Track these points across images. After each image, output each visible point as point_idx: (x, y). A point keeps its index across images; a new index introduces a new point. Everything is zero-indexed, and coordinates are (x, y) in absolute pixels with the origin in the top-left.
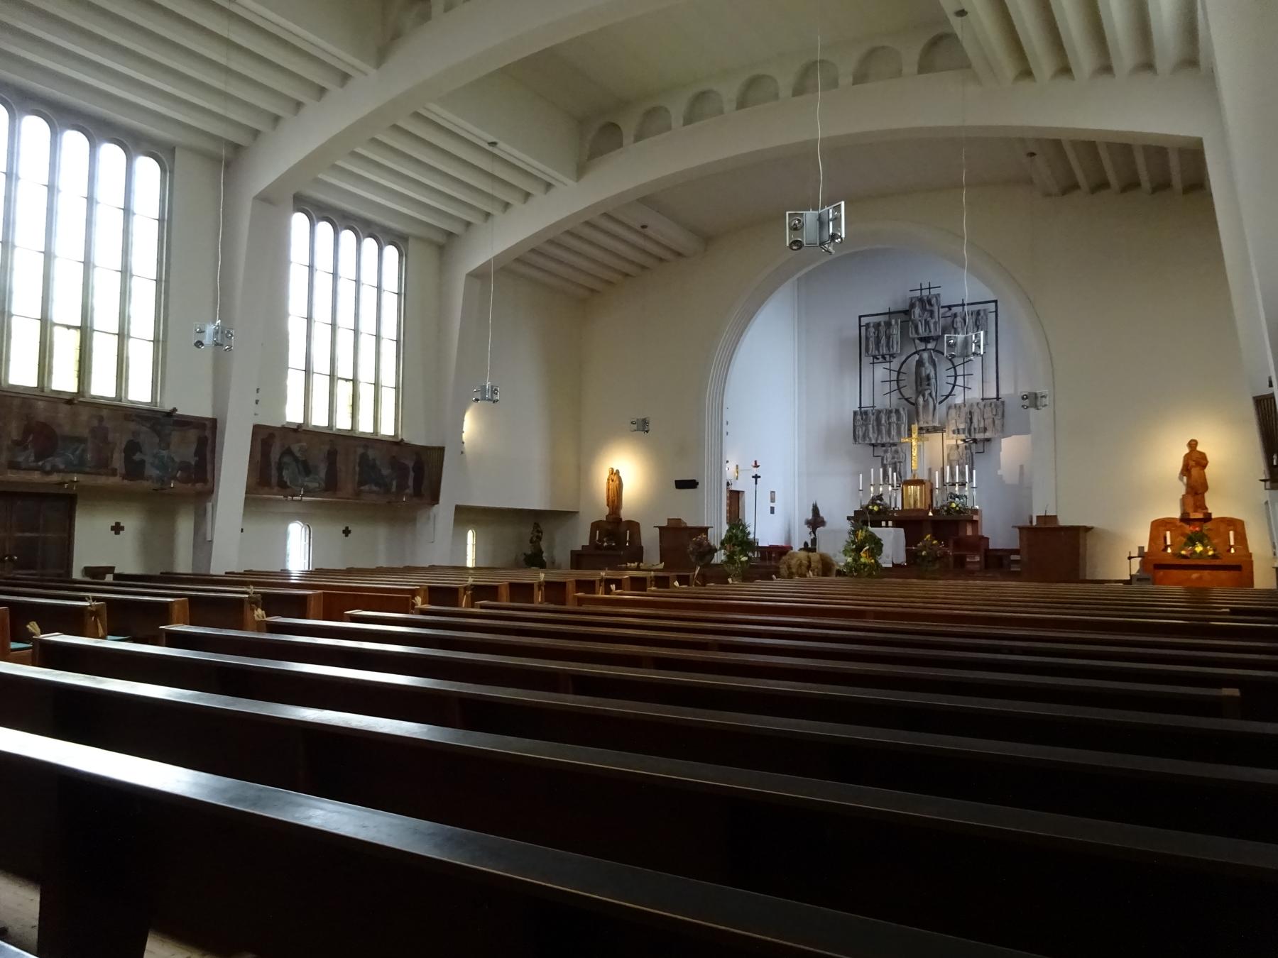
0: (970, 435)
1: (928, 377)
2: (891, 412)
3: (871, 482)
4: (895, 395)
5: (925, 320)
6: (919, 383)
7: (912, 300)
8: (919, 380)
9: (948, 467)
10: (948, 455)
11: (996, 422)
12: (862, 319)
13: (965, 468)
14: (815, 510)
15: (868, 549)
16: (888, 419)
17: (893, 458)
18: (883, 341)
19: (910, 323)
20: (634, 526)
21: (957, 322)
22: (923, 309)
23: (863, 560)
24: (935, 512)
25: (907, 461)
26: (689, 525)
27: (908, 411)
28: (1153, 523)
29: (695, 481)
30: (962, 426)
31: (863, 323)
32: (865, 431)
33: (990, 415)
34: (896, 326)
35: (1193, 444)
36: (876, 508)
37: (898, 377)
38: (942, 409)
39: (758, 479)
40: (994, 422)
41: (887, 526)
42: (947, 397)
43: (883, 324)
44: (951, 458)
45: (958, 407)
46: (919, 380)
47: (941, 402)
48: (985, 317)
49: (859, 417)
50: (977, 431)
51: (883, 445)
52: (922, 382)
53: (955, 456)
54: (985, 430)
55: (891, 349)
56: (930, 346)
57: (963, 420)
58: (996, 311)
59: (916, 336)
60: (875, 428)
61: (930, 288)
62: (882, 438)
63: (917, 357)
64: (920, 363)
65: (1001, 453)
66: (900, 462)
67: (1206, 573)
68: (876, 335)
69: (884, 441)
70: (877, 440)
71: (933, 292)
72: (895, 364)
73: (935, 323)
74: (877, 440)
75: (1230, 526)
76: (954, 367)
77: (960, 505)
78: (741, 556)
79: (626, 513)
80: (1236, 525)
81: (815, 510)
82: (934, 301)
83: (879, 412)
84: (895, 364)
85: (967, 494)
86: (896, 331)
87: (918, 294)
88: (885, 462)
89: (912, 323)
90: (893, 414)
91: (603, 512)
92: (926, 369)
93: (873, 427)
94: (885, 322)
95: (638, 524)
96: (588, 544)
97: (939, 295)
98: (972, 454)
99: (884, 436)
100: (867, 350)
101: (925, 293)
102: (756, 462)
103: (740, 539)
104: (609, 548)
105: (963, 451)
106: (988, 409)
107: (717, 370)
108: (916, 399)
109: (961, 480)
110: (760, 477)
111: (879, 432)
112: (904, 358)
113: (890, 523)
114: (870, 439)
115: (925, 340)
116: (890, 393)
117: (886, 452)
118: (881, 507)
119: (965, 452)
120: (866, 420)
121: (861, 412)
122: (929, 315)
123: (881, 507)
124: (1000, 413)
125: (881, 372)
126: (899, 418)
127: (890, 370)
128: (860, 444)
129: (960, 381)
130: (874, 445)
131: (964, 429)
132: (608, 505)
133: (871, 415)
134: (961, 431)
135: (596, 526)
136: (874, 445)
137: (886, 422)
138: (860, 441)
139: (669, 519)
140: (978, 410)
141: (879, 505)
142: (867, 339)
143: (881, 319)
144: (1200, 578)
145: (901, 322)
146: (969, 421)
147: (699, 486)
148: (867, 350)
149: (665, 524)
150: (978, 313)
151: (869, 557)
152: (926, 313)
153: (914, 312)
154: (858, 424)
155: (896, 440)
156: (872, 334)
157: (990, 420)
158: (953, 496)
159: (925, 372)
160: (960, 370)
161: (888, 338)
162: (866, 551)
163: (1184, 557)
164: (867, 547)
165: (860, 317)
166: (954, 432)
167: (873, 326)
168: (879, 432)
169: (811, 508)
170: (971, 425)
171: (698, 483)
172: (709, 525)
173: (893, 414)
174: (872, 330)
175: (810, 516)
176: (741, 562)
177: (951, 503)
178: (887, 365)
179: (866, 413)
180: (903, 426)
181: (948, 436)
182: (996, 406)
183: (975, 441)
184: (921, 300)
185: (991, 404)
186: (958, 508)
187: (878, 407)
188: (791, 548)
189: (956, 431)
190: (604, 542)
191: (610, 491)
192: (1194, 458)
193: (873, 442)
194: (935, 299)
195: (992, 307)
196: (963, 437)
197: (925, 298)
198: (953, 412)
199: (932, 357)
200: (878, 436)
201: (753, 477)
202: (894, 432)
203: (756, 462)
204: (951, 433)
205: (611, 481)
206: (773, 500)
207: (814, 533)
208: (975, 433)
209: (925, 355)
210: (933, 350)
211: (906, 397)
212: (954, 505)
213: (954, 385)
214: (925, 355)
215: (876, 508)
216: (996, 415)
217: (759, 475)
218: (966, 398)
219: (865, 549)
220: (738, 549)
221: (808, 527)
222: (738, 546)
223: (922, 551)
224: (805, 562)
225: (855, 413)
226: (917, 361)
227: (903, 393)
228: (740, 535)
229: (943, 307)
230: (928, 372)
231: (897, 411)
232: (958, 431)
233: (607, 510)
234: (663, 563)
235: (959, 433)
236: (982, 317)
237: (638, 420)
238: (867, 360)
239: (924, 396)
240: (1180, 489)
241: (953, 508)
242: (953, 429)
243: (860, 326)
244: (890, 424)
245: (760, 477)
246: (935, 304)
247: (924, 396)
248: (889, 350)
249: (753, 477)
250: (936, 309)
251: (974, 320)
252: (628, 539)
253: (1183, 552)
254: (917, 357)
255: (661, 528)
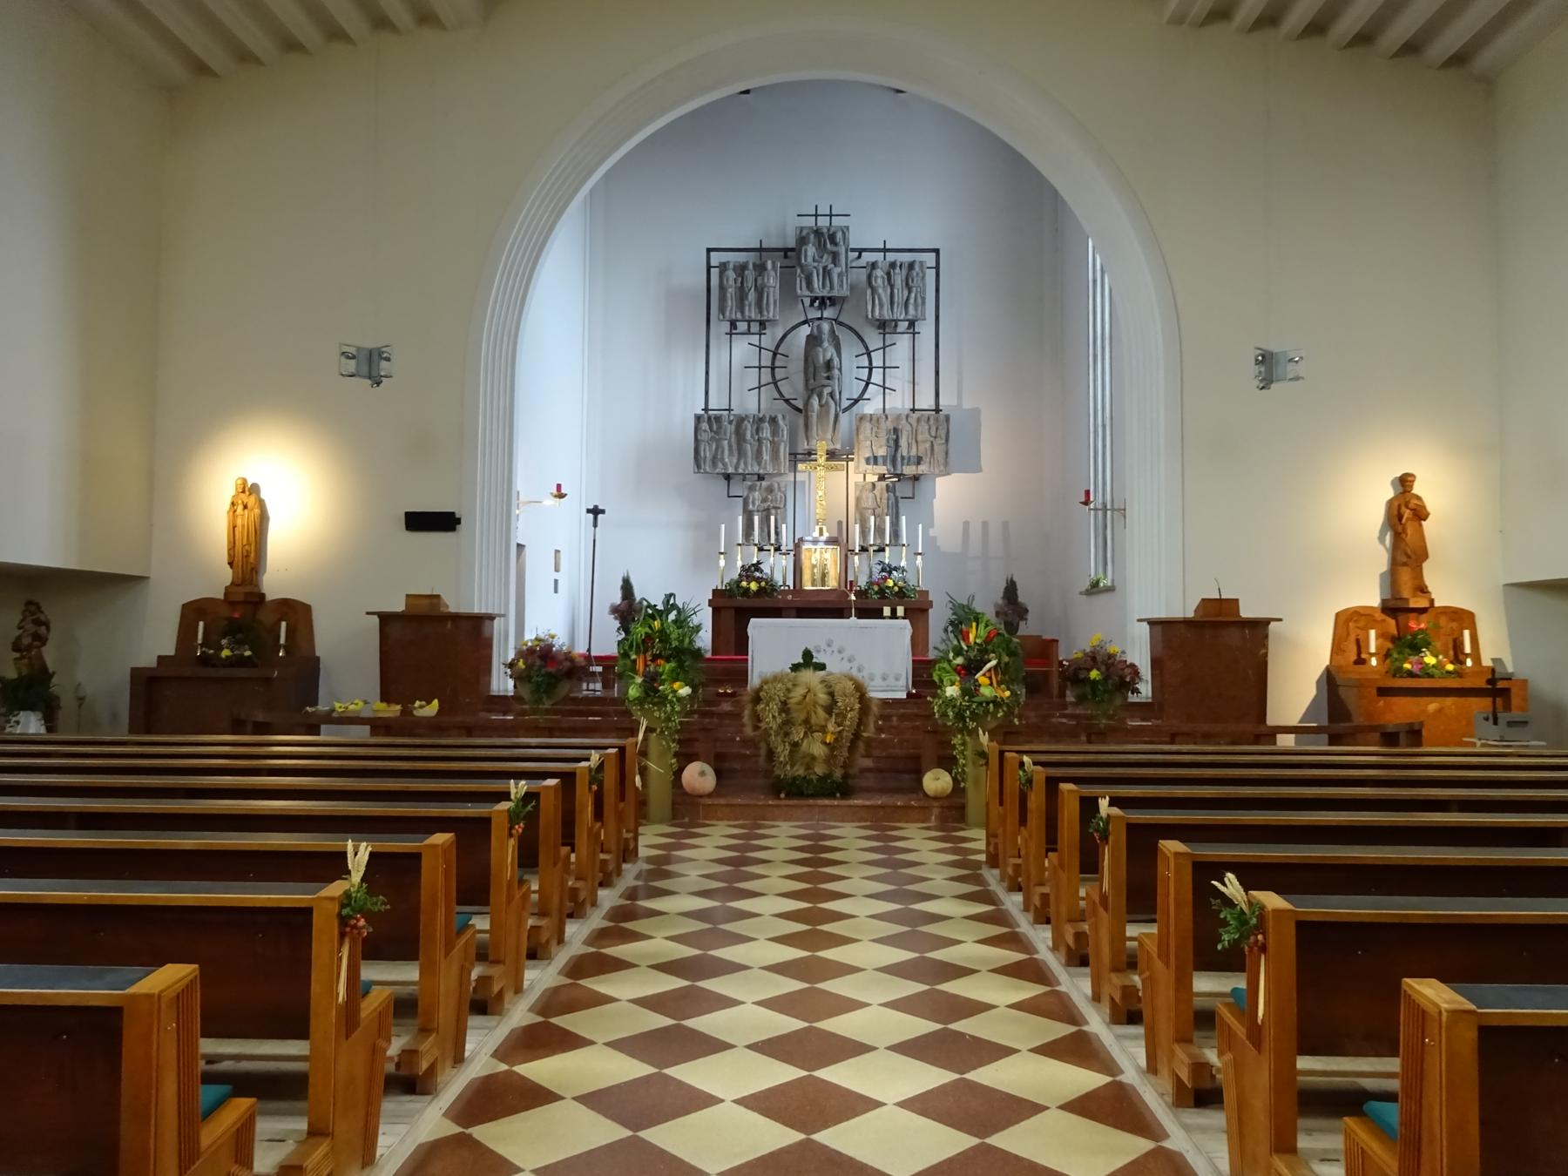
0: (894, 466)
1: (829, 365)
2: (761, 420)
3: (719, 547)
4: (768, 392)
5: (825, 268)
7: (801, 231)
8: (811, 369)
9: (857, 526)
10: (858, 500)
11: (936, 447)
12: (712, 254)
13: (884, 521)
15: (995, 667)
17: (764, 500)
18: (752, 296)
20: (296, 612)
21: (876, 277)
22: (821, 247)
23: (987, 691)
24: (859, 594)
25: (788, 503)
26: (453, 608)
27: (790, 422)
28: (1338, 615)
29: (453, 514)
30: (882, 452)
34: (773, 273)
35: (1405, 482)
36: (754, 586)
37: (773, 362)
39: (600, 516)
41: (894, 615)
42: (856, 401)
43: (751, 266)
44: (864, 505)
45: (874, 418)
46: (811, 369)
48: (921, 275)
49: (705, 426)
50: (906, 461)
51: (744, 477)
52: (818, 373)
53: (869, 502)
54: (919, 460)
55: (765, 313)
56: (829, 313)
57: (883, 440)
58: (937, 268)
59: (808, 293)
60: (735, 447)
62: (746, 464)
64: (813, 341)
65: (935, 501)
66: (776, 508)
67: (1449, 701)
68: (739, 284)
69: (750, 470)
70: (736, 468)
71: (837, 221)
72: (768, 341)
73: (840, 275)
74: (736, 468)
75: (1454, 620)
77: (901, 583)
78: (676, 686)
79: (276, 581)
80: (1463, 618)
82: (839, 236)
83: (741, 420)
85: (903, 563)
86: (772, 281)
87: (810, 222)
88: (751, 507)
89: (802, 272)
90: (766, 425)
91: (216, 579)
92: (825, 350)
93: (730, 446)
95: (307, 609)
96: (172, 653)
97: (847, 228)
98: (896, 498)
99: (749, 460)
100: (722, 310)
101: (823, 222)
102: (559, 487)
103: (675, 644)
104: (237, 662)
105: (881, 494)
106: (924, 427)
107: (508, 279)
108: (807, 403)
109: (878, 541)
110: (603, 512)
111: (741, 453)
113: (900, 611)
114: (725, 465)
115: (823, 302)
116: (759, 388)
117: (752, 489)
121: (709, 418)
122: (830, 260)
123: (763, 584)
124: (942, 433)
125: (743, 350)
126: (775, 432)
127: (760, 348)
128: (706, 472)
129: (877, 377)
130: (728, 477)
131: (884, 458)
132: (231, 564)
133: (726, 423)
134: (880, 461)
135: (193, 611)
136: (728, 477)
138: (708, 469)
139: (408, 596)
140: (909, 428)
141: (758, 580)
142: (722, 288)
143: (750, 258)
144: (1440, 711)
145: (780, 267)
146: (892, 443)
147: (462, 527)
149: (399, 606)
150: (911, 266)
151: (999, 684)
152: (825, 256)
153: (806, 251)
154: (704, 436)
155: (770, 469)
156: (731, 282)
157: (928, 445)
158: (888, 570)
159: (824, 357)
160: (877, 359)
161: (760, 292)
162: (990, 670)
163: (1411, 674)
164: (994, 663)
165: (709, 251)
167: (734, 270)
168: (741, 453)
170: (896, 450)
171: (458, 521)
172: (496, 612)
174: (731, 274)
176: (680, 699)
177: (885, 579)
178: (755, 339)
179: (718, 419)
180: (783, 445)
181: (857, 467)
182: (937, 420)
183: (899, 476)
184: (818, 232)
185: (929, 418)
186: (896, 589)
187: (737, 410)
189: (872, 461)
190: (221, 648)
191: (238, 530)
192: (1411, 506)
193: (731, 470)
194: (841, 233)
196: (882, 469)
197: (825, 230)
198: (867, 426)
199: (834, 332)
200: (739, 460)
201: (589, 511)
202: (766, 457)
203: (559, 487)
205: (240, 509)
208: (902, 464)
209: (826, 327)
210: (835, 320)
211: (787, 397)
212: (890, 583)
214: (826, 327)
215: (754, 586)
216: (935, 437)
217: (600, 507)
218: (887, 407)
219: (989, 666)
220: (667, 667)
222: (668, 661)
223: (1089, 670)
224: (823, 697)
225: (698, 418)
227: (782, 389)
228: (674, 633)
231: (773, 420)
232: (875, 460)
233: (226, 575)
234: (436, 702)
235: (876, 463)
237: (359, 349)
239: (820, 396)
240: (1380, 559)
241: (888, 587)
242: (867, 455)
245: (603, 512)
246: (842, 243)
247: (820, 396)
248: (761, 312)
249: (589, 511)
251: (904, 278)
252: (282, 641)
253: (1407, 666)
254: (805, 330)
255: (386, 619)
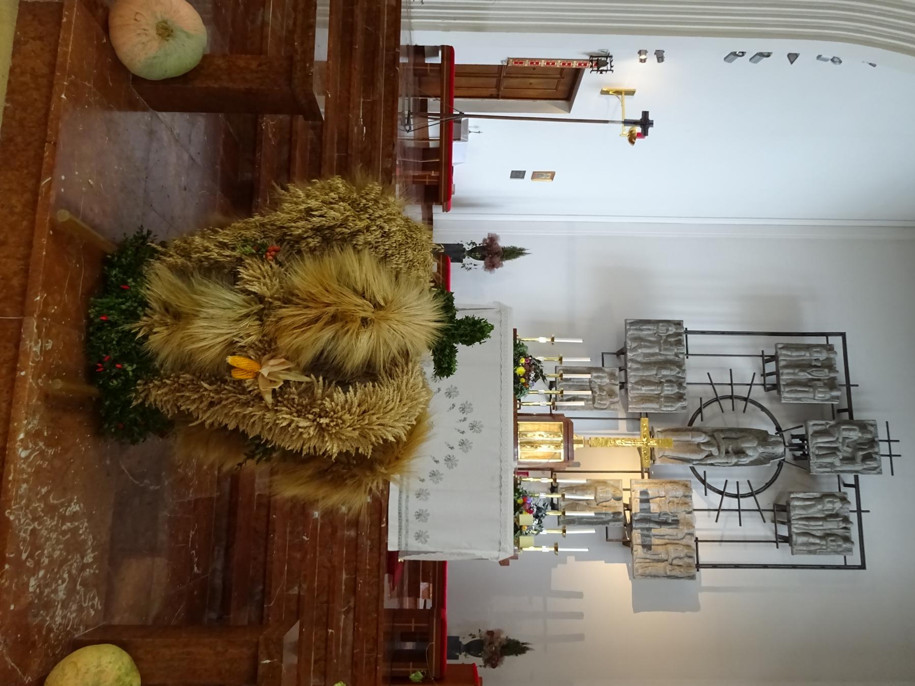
0: (638, 521)
2: (680, 385)
5: (836, 448)
6: (728, 435)
7: (872, 425)
8: (734, 435)
9: (584, 481)
10: (604, 483)
14: (514, 253)
16: (668, 381)
17: (601, 388)
18: (804, 376)
19: (832, 423)
22: (858, 446)
25: (595, 411)
31: (832, 340)
32: (650, 342)
33: (673, 555)
38: (683, 470)
40: (659, 561)
45: (688, 500)
46: (734, 435)
47: (693, 469)
48: (840, 549)
49: (672, 330)
50: (645, 532)
54: (647, 547)
55: (787, 389)
57: (666, 509)
58: (846, 567)
59: (810, 432)
61: (890, 456)
62: (637, 369)
63: (772, 431)
64: (762, 437)
68: (814, 363)
69: (631, 373)
70: (632, 360)
71: (885, 461)
73: (832, 465)
74: (632, 360)
76: (751, 494)
81: (514, 253)
83: (680, 365)
84: (758, 393)
86: (820, 396)
87: (882, 435)
90: (676, 390)
92: (755, 448)
93: (653, 355)
94: (834, 379)
97: (880, 473)
100: (787, 347)
101: (883, 448)
106: (682, 552)
108: (699, 431)
111: (647, 365)
112: (766, 404)
114: (635, 349)
116: (711, 384)
117: (612, 375)
118: (523, 380)
119: (610, 511)
120: (666, 342)
121: (680, 334)
122: (846, 455)
124: (677, 572)
127: (751, 385)
128: (626, 331)
131: (648, 510)
134: (645, 506)
137: (664, 376)
140: (680, 536)
142: (808, 347)
146: (663, 518)
148: (787, 347)
152: (850, 450)
154: (662, 329)
156: (816, 356)
157: (663, 556)
165: (843, 335)
166: (644, 493)
167: (828, 359)
168: (647, 365)
169: (519, 246)
173: (676, 390)
174: (823, 356)
175: (503, 243)
179: (679, 343)
183: (629, 527)
184: (873, 442)
185: (690, 557)
187: (690, 362)
188: (447, 209)
189: (644, 497)
195: (854, 559)
196: (636, 507)
197: (876, 450)
198: (680, 492)
201: (645, 114)
202: (645, 390)
204: (644, 488)
206: (536, 175)
207: (473, 251)
208: (642, 529)
211: (704, 411)
213: (722, 493)
221: (485, 240)
225: (679, 324)
226: (766, 432)
229: (856, 478)
230: (749, 452)
231: (680, 397)
235: (642, 501)
236: (840, 546)
238: (768, 346)
239: (707, 444)
242: (649, 492)
243: (826, 335)
244: (660, 383)
246: (865, 467)
247: (707, 444)
248: (787, 385)
249: (645, 114)
250: (858, 467)
251: (835, 531)
254: (772, 431)
